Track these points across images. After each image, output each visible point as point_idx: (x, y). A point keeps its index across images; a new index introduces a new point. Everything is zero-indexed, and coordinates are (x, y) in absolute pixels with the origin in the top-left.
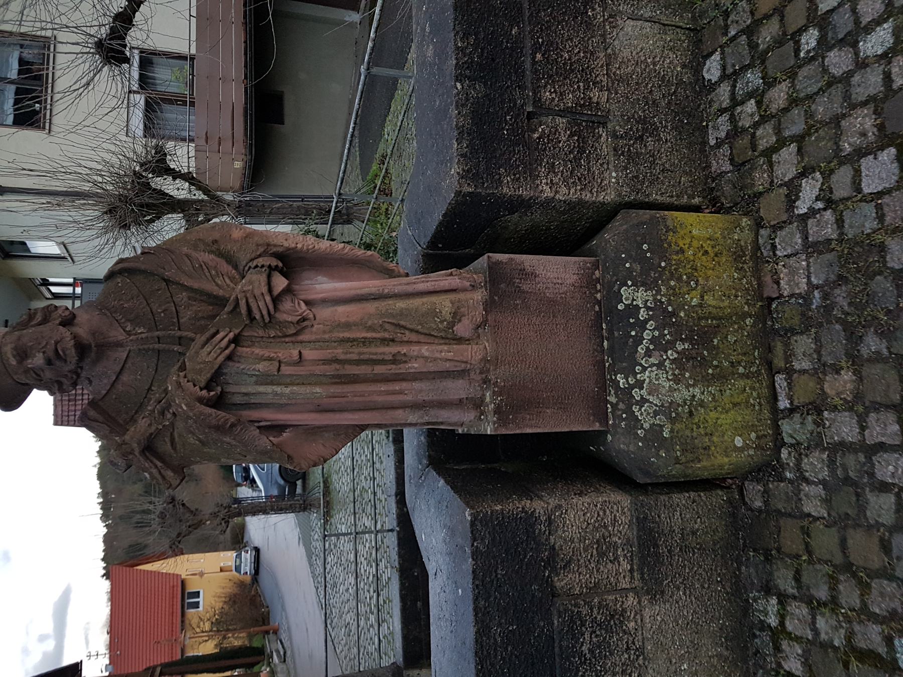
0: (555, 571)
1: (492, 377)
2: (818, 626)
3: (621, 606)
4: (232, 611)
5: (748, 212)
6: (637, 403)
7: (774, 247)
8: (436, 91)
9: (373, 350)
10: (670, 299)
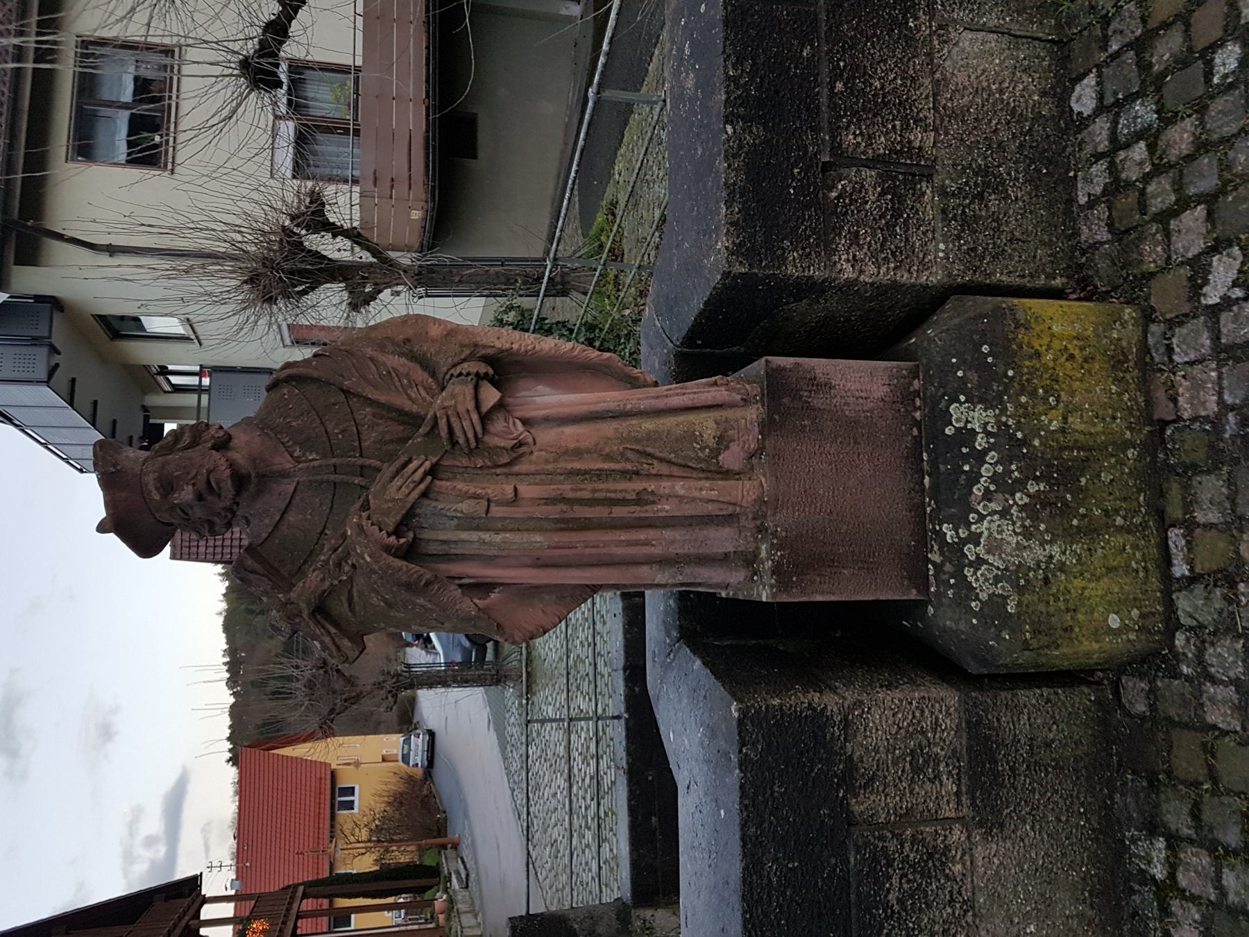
0: (852, 790)
1: (769, 524)
2: (1224, 882)
3: (943, 841)
4: (397, 816)
5: (1134, 300)
6: (971, 564)
7: (1170, 350)
8: (698, 135)
9: (611, 485)
10: (1019, 422)
